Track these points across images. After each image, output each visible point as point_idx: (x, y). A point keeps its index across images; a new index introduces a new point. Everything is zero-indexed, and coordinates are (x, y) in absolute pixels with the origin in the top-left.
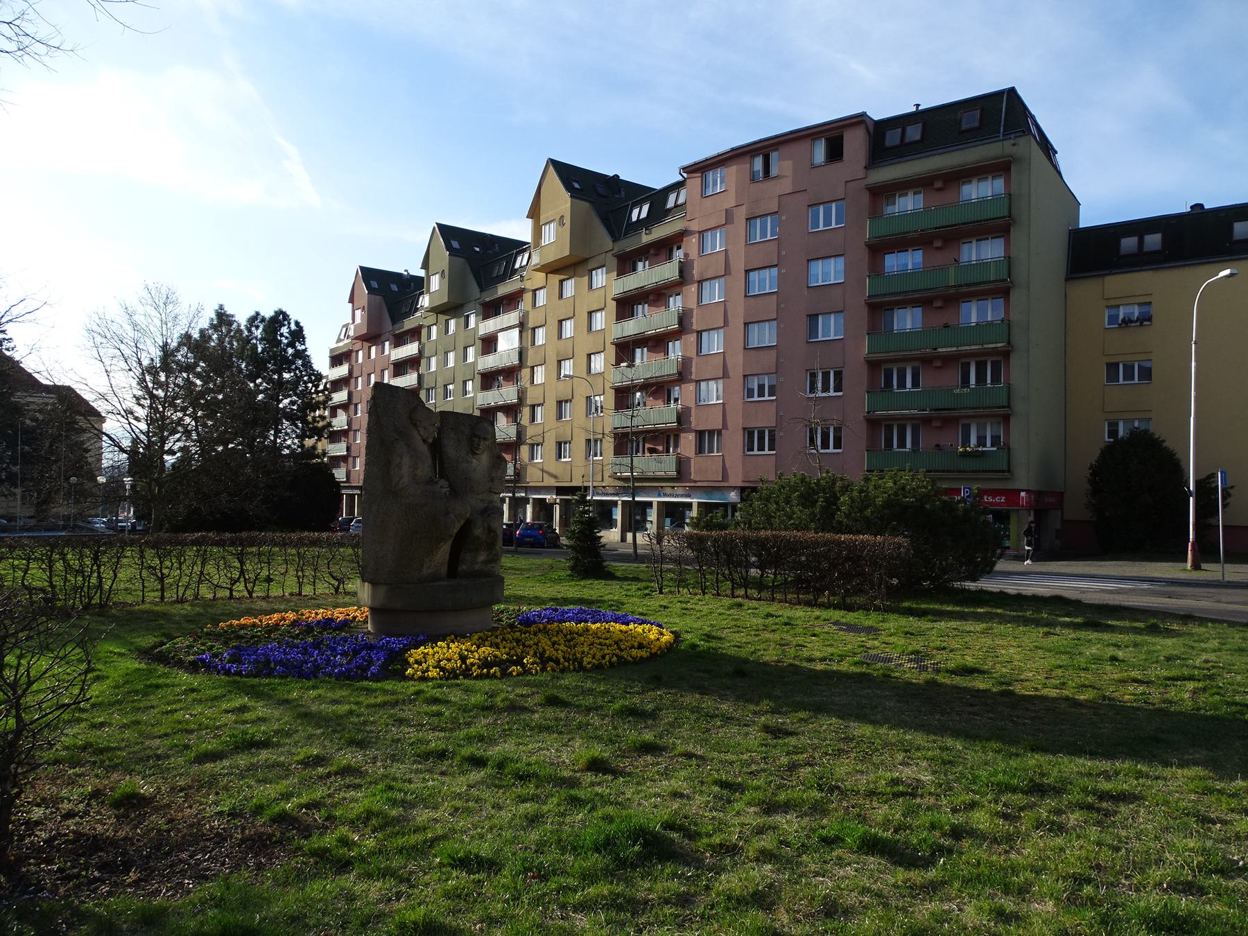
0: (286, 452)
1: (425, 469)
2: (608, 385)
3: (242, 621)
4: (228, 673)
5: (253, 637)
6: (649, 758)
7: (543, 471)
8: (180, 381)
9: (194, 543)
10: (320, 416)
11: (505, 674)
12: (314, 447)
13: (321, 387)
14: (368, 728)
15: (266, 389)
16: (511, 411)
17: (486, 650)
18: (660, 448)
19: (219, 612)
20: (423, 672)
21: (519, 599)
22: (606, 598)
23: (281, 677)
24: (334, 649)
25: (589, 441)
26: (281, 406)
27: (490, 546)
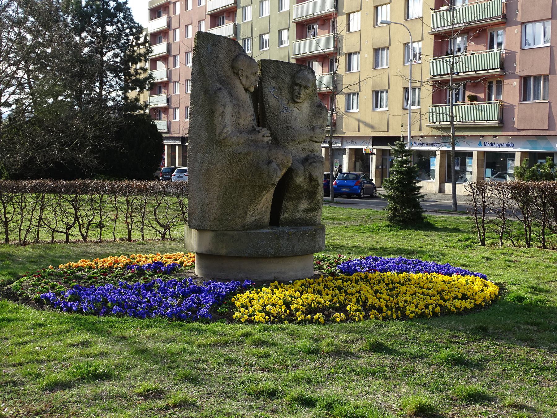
0: (110, 103)
1: (248, 117)
2: (427, 30)
3: (80, 263)
4: (70, 310)
5: (90, 278)
6: (477, 407)
7: (359, 121)
8: (12, 35)
9: (34, 189)
10: (141, 68)
11: (328, 320)
12: (137, 100)
13: (142, 40)
14: (201, 366)
15: (91, 42)
16: (327, 59)
17: (309, 297)
18: (481, 96)
19: (58, 254)
20: (250, 316)
21: (338, 248)
22: (426, 249)
23: (119, 316)
24: (165, 292)
25: (406, 89)
26: (105, 58)
27: (312, 195)
